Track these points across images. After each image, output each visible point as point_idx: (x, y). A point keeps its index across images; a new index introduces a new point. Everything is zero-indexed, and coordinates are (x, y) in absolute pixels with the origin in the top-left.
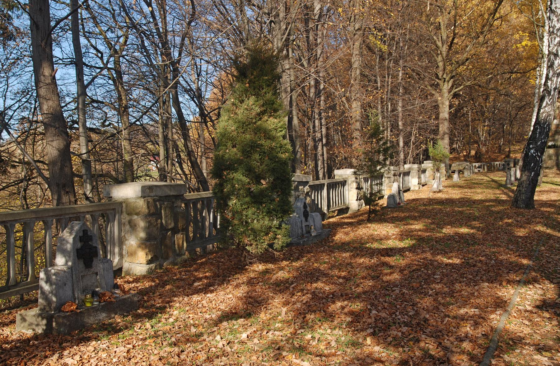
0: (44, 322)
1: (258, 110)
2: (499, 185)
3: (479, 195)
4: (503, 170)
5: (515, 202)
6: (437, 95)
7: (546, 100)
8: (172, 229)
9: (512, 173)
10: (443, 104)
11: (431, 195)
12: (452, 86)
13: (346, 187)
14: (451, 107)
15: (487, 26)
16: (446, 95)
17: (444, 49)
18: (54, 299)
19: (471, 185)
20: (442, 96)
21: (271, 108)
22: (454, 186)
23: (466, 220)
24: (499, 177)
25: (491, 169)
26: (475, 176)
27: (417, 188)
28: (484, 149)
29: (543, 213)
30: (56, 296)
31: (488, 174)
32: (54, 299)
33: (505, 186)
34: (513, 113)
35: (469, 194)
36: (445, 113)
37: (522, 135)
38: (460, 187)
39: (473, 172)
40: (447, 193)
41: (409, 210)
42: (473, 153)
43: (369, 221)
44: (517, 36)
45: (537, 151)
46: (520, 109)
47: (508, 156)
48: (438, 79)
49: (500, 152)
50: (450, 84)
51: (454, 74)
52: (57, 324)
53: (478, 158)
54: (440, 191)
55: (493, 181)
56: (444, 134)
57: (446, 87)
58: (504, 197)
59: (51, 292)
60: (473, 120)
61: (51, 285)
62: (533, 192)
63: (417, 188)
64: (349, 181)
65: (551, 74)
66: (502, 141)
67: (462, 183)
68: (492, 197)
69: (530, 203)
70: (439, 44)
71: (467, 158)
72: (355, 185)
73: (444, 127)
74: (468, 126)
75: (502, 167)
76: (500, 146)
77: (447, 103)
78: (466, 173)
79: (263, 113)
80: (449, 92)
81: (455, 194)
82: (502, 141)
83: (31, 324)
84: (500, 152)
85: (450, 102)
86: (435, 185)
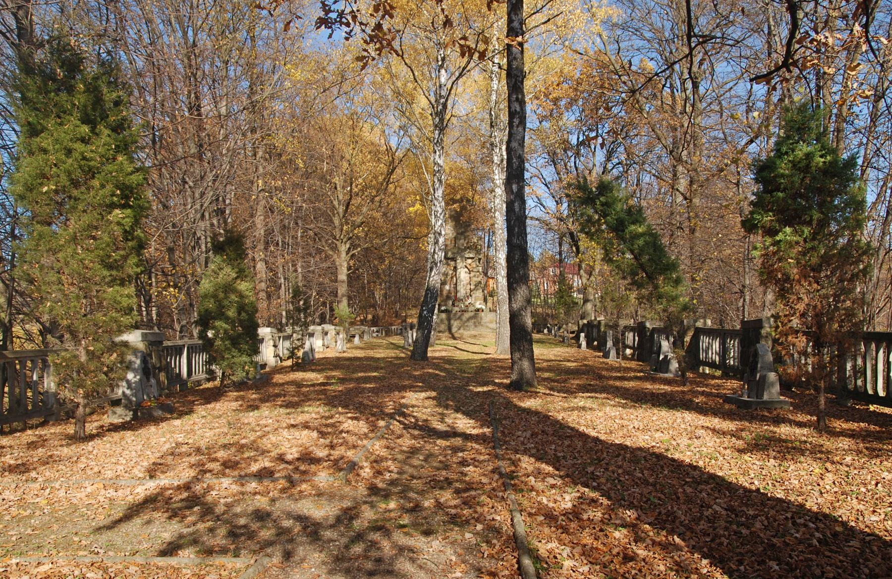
0: (131, 413)
1: (234, 275)
2: (396, 347)
3: (380, 354)
4: (401, 334)
5: (413, 356)
6: (335, 256)
7: (434, 270)
8: (158, 368)
9: (410, 335)
10: (341, 265)
11: (338, 355)
12: (349, 248)
13: (264, 344)
14: (349, 268)
15: (382, 188)
16: (344, 255)
17: (341, 209)
18: (134, 399)
19: (372, 347)
20: (339, 257)
21: (241, 275)
22: (357, 348)
23: (376, 369)
24: (397, 340)
25: (388, 333)
26: (375, 340)
27: (321, 350)
28: (381, 313)
29: (434, 363)
30: (136, 397)
31: (387, 338)
32: (134, 399)
33: (403, 347)
34: (408, 277)
35: (371, 353)
36: (343, 276)
37: (418, 299)
38: (362, 348)
39: (371, 335)
40: (352, 353)
41: (323, 364)
42: (370, 317)
43: (293, 371)
44: (409, 200)
45: (428, 312)
46: (415, 272)
47: (405, 321)
48: (335, 238)
49: (396, 317)
50: (348, 246)
51: (351, 235)
52: (142, 413)
53: (375, 322)
54: (344, 352)
55: (392, 344)
56: (343, 296)
57: (344, 248)
58: (403, 355)
59: (132, 395)
60: (369, 283)
61: (132, 390)
62: (426, 352)
63: (321, 350)
64: (266, 339)
65: (437, 249)
66: (398, 306)
67: (362, 345)
68: (393, 355)
69: (424, 356)
70: (336, 203)
71: (362, 322)
72: (272, 343)
73: (342, 289)
74: (364, 288)
75: (399, 331)
76: (397, 312)
77: (345, 265)
78: (366, 337)
79: (236, 278)
80: (347, 254)
81: (360, 354)
82: (398, 306)
83: (120, 416)
84: (396, 317)
85: (348, 264)
86: (339, 346)
